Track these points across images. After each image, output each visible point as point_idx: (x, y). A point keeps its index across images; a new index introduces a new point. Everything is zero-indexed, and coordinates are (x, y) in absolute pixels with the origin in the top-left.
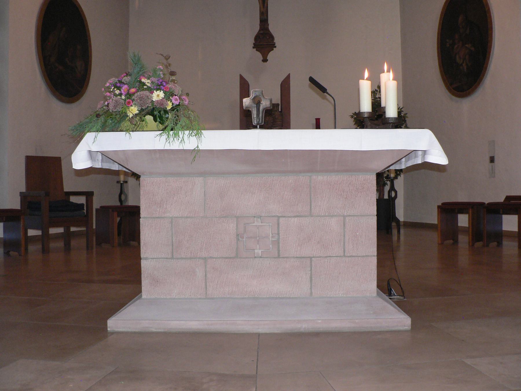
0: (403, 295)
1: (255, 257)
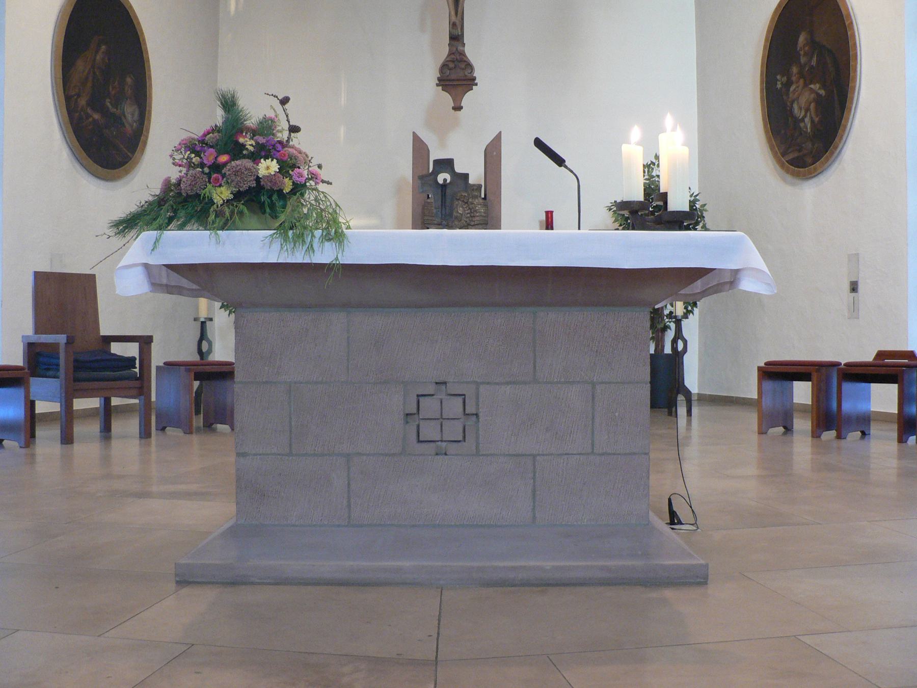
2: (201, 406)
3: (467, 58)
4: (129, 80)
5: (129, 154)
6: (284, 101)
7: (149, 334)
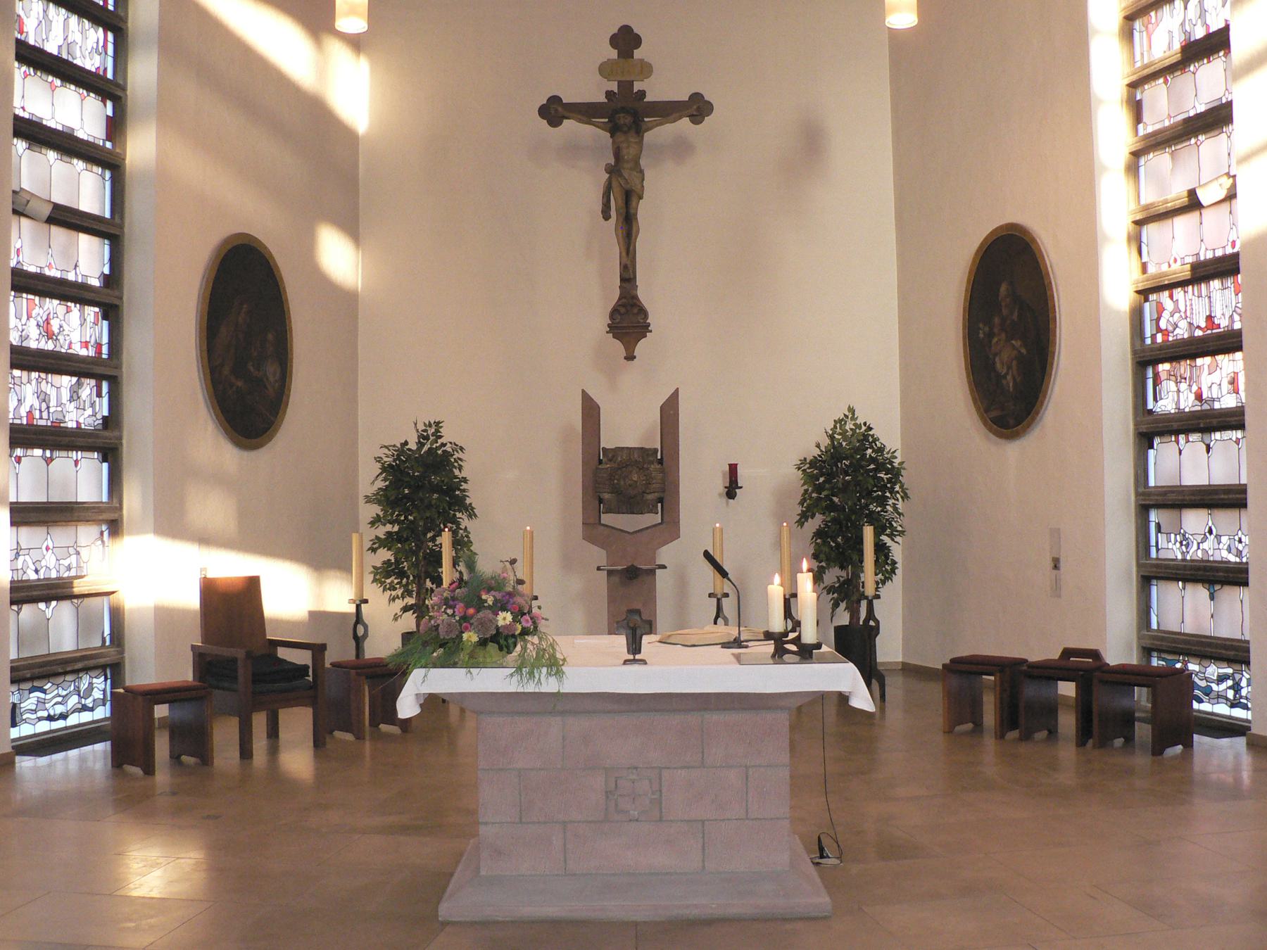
0: (841, 857)
1: (631, 820)
2: (370, 714)
3: (641, 302)
4: (270, 336)
5: (272, 418)
6: (513, 562)
7: (324, 642)
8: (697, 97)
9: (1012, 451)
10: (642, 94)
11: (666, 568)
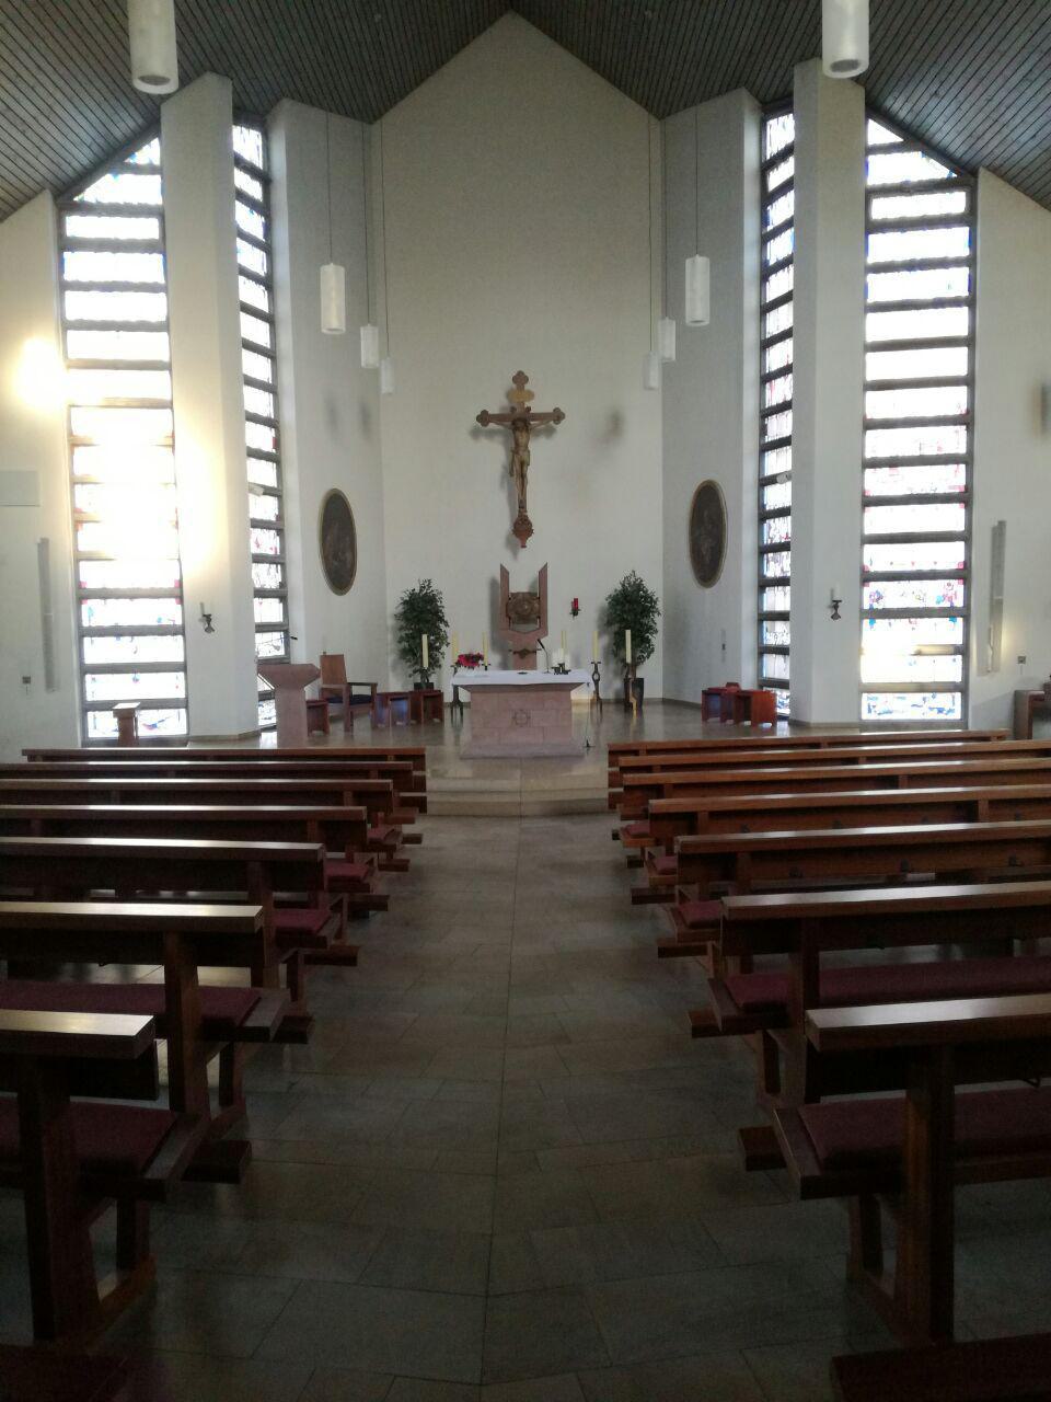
8: (557, 410)
9: (708, 591)
10: (529, 409)
11: (1002, 524)
